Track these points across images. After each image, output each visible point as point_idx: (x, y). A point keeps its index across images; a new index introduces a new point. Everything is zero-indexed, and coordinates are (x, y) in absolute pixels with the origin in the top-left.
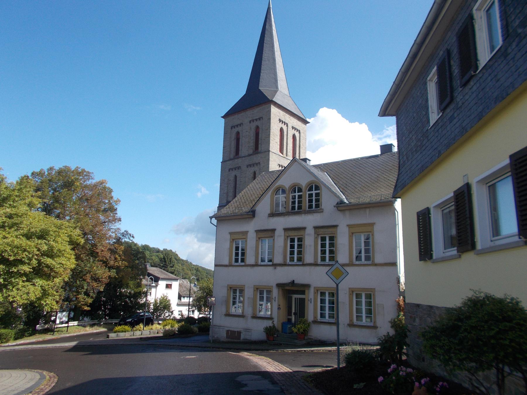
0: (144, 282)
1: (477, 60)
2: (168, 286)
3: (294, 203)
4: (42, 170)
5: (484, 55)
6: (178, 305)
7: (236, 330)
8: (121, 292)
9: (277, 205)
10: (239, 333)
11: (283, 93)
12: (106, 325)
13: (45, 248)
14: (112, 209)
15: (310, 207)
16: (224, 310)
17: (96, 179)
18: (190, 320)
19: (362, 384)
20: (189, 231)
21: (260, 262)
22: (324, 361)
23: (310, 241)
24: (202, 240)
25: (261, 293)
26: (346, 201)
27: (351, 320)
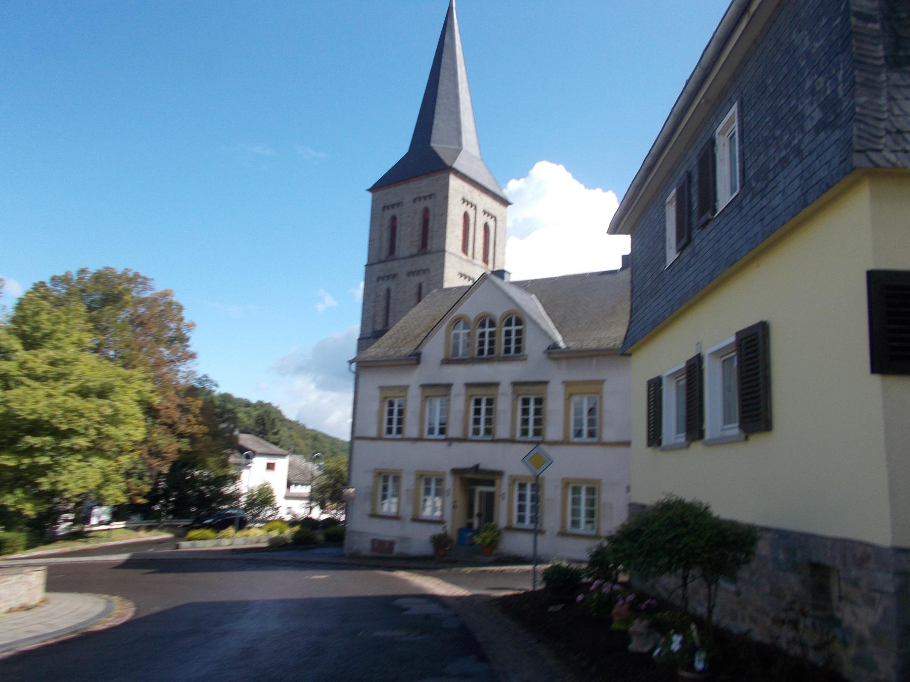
0: (232, 459)
1: (715, 200)
2: (270, 466)
3: (482, 343)
4: (68, 273)
5: (724, 197)
6: (287, 497)
7: (387, 539)
8: (193, 476)
9: (456, 347)
10: (391, 544)
11: (470, 156)
12: (170, 528)
13: (109, 411)
14: (182, 339)
15: (507, 351)
16: (367, 507)
17: (159, 287)
18: (308, 522)
19: (560, 607)
20: (301, 369)
21: (426, 435)
22: (518, 580)
23: (504, 403)
24: (323, 386)
25: (428, 482)
26: (562, 345)
27: (563, 526)
